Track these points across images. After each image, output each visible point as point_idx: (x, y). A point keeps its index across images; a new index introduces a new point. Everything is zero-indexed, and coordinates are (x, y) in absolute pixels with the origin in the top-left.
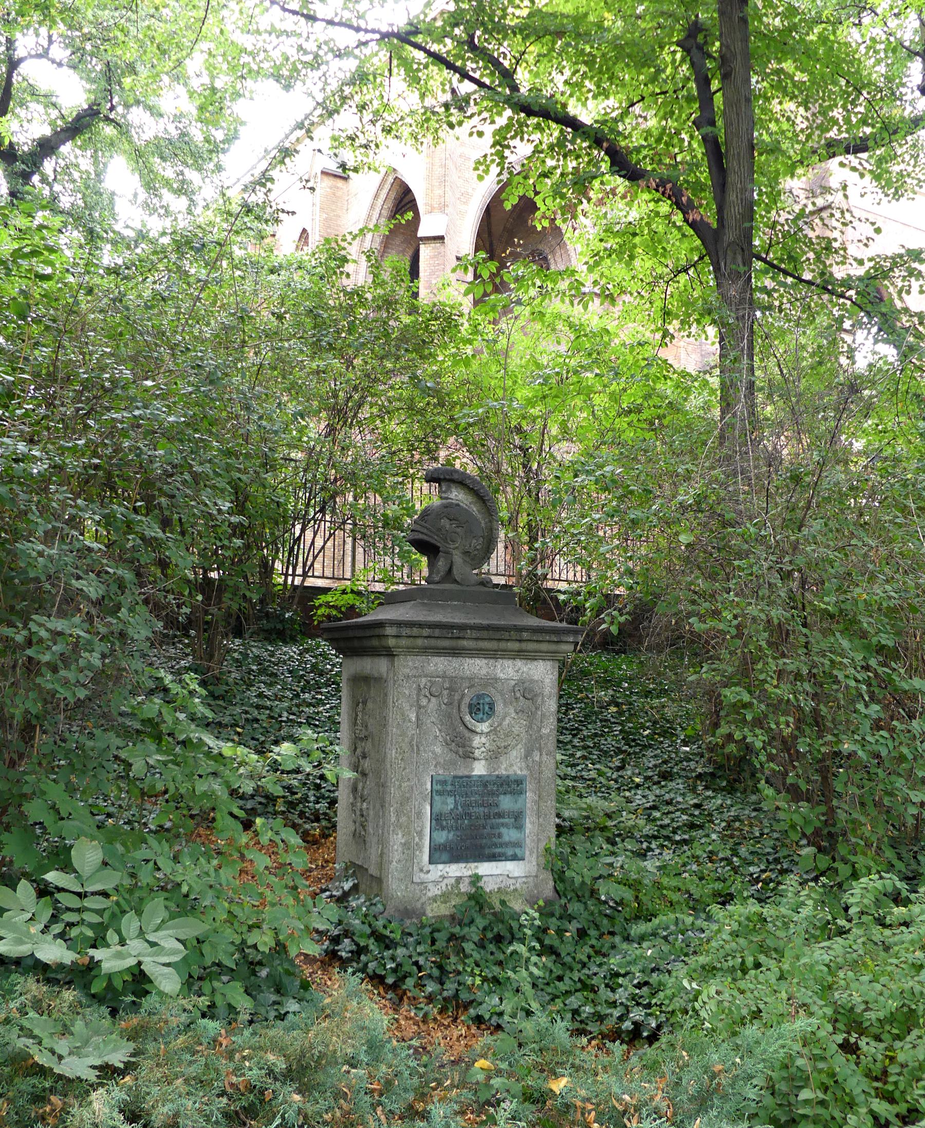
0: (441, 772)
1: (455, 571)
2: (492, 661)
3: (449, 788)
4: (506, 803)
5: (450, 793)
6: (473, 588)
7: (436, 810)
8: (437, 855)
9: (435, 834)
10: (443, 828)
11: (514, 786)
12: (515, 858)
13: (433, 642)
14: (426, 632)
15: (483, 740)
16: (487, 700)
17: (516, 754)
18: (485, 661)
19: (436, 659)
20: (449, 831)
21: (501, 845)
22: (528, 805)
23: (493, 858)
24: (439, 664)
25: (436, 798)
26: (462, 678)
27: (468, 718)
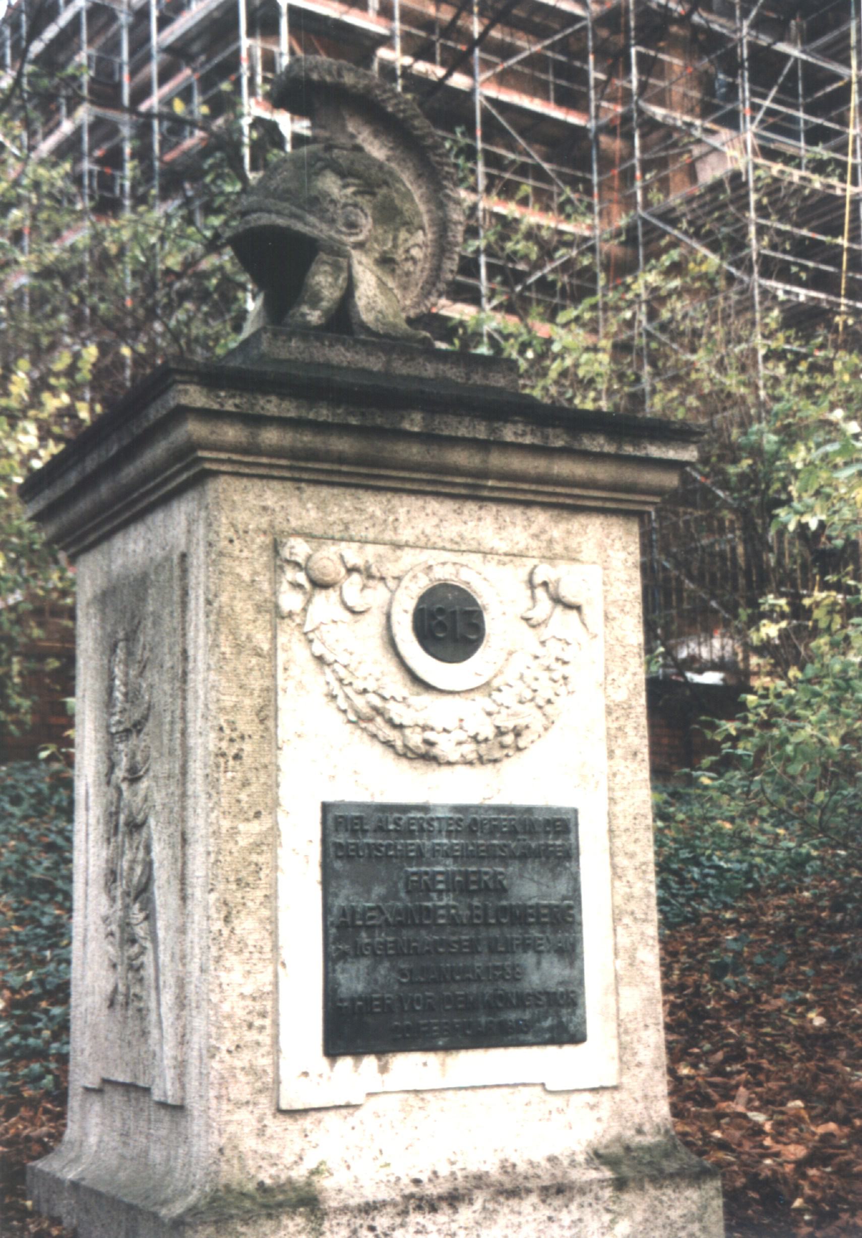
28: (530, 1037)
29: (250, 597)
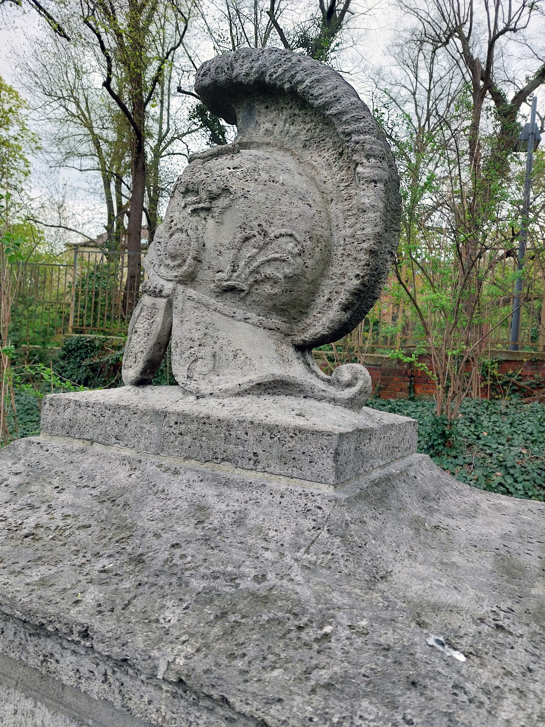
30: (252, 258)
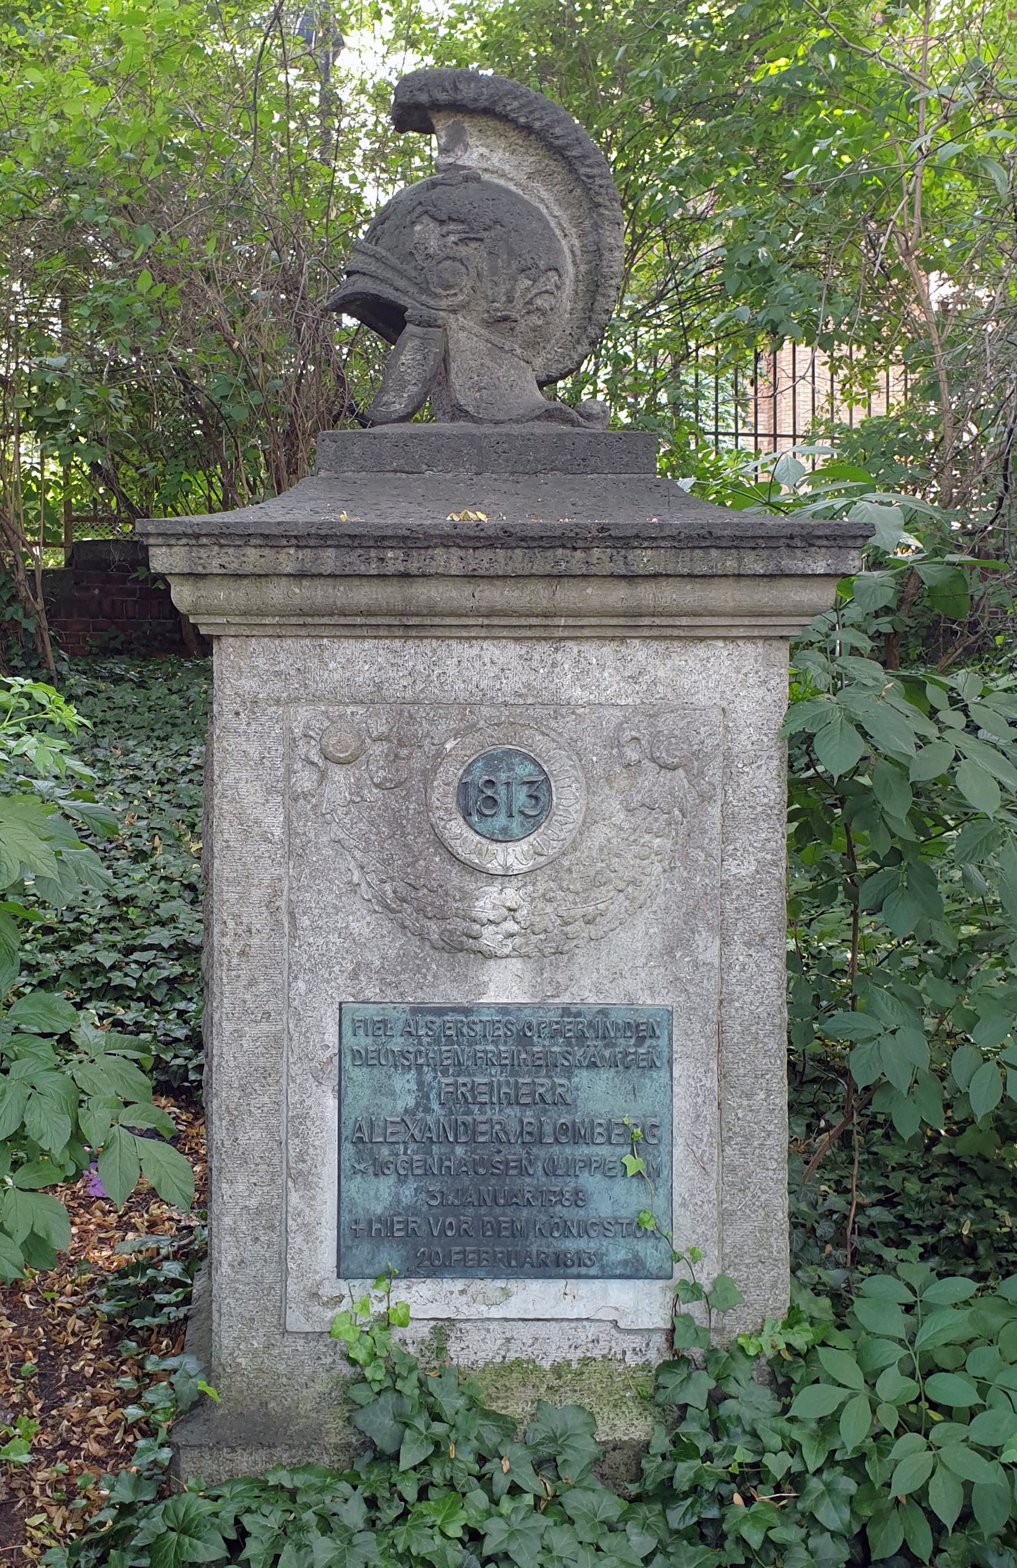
0: (371, 992)
1: (457, 380)
2: (542, 649)
3: (397, 1044)
4: (598, 1093)
5: (400, 1061)
6: (516, 429)
7: (355, 1113)
8: (362, 1251)
9: (354, 1186)
10: (380, 1169)
11: (626, 1044)
12: (634, 1270)
13: (319, 593)
14: (288, 560)
15: (511, 896)
16: (524, 771)
17: (638, 938)
18: (514, 650)
19: (350, 648)
20: (402, 1180)
21: (584, 1230)
22: (680, 1104)
23: (556, 1266)
24: (357, 662)
25: (358, 1074)
26: (436, 704)
27: (456, 828)
28: (593, 1271)
29: (258, 778)
30: (528, 289)
